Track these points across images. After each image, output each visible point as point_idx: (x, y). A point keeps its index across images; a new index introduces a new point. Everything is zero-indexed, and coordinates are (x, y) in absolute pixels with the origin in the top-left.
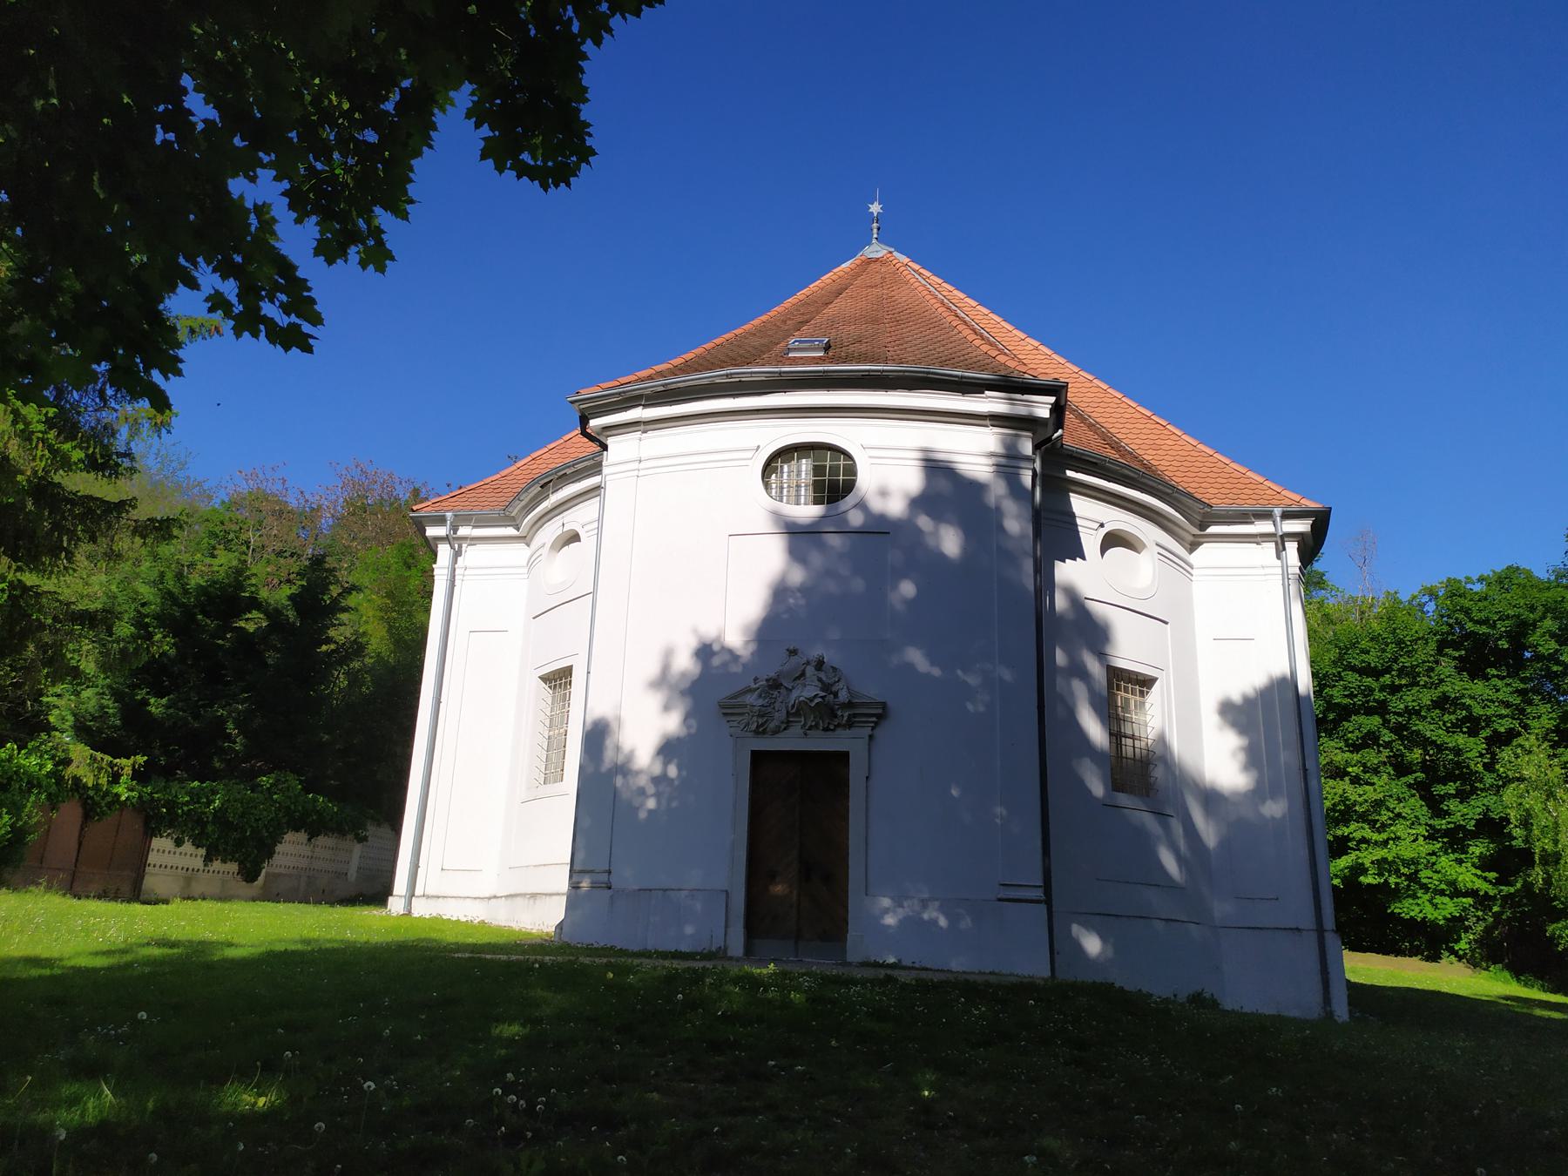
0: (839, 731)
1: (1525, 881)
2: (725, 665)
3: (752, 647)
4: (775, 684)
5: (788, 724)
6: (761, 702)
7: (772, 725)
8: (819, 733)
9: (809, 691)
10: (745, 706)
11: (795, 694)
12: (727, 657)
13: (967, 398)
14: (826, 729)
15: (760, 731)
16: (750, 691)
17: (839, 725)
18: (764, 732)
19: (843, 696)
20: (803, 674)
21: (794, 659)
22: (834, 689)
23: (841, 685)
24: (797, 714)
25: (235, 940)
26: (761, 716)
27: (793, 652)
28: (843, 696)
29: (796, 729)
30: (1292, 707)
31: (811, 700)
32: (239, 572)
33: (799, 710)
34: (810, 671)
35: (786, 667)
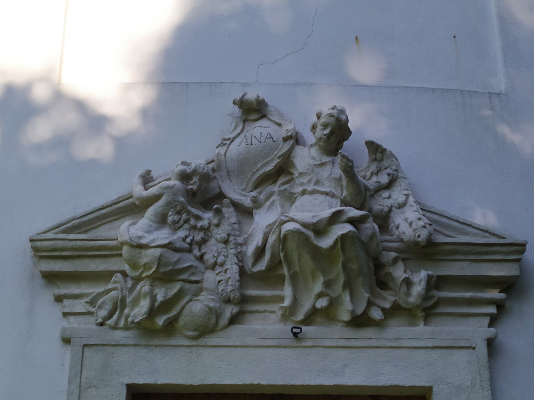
0: (398, 330)
1: (505, 300)
2: (62, 142)
3: (140, 97)
4: (200, 192)
5: (241, 307)
6: (163, 236)
7: (197, 307)
8: (337, 333)
9: (313, 203)
10: (112, 252)
11: (264, 219)
12: (70, 119)
13: (257, 178)
14: (360, 321)
15: (159, 327)
16: (132, 208)
17: (395, 311)
18: (170, 328)
19: (408, 224)
20: (284, 169)
21: (259, 129)
22: (381, 203)
23: (397, 195)
24: (271, 277)
25: (398, 159)
26: (165, 275)
27: (253, 110)
28: (408, 224)
29: (267, 323)
30: (524, 243)
31: (319, 229)
32: (204, 219)
33: (274, 266)
34: (305, 158)
35: (235, 149)
